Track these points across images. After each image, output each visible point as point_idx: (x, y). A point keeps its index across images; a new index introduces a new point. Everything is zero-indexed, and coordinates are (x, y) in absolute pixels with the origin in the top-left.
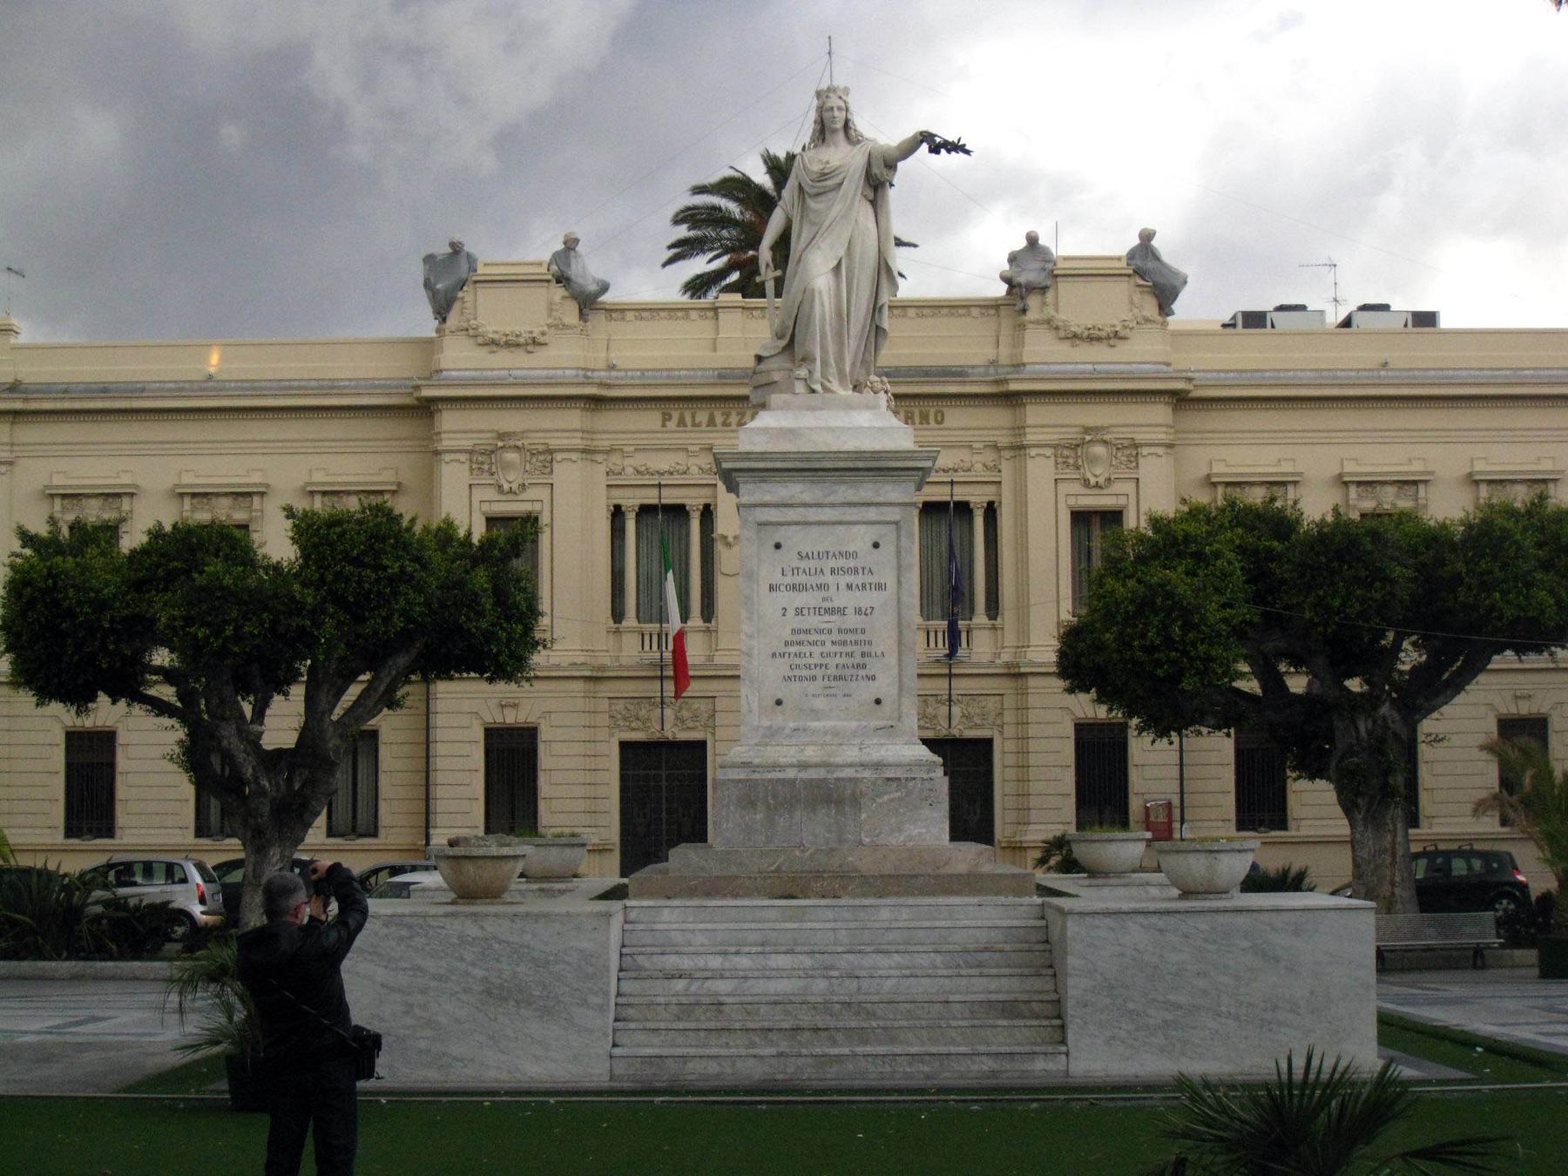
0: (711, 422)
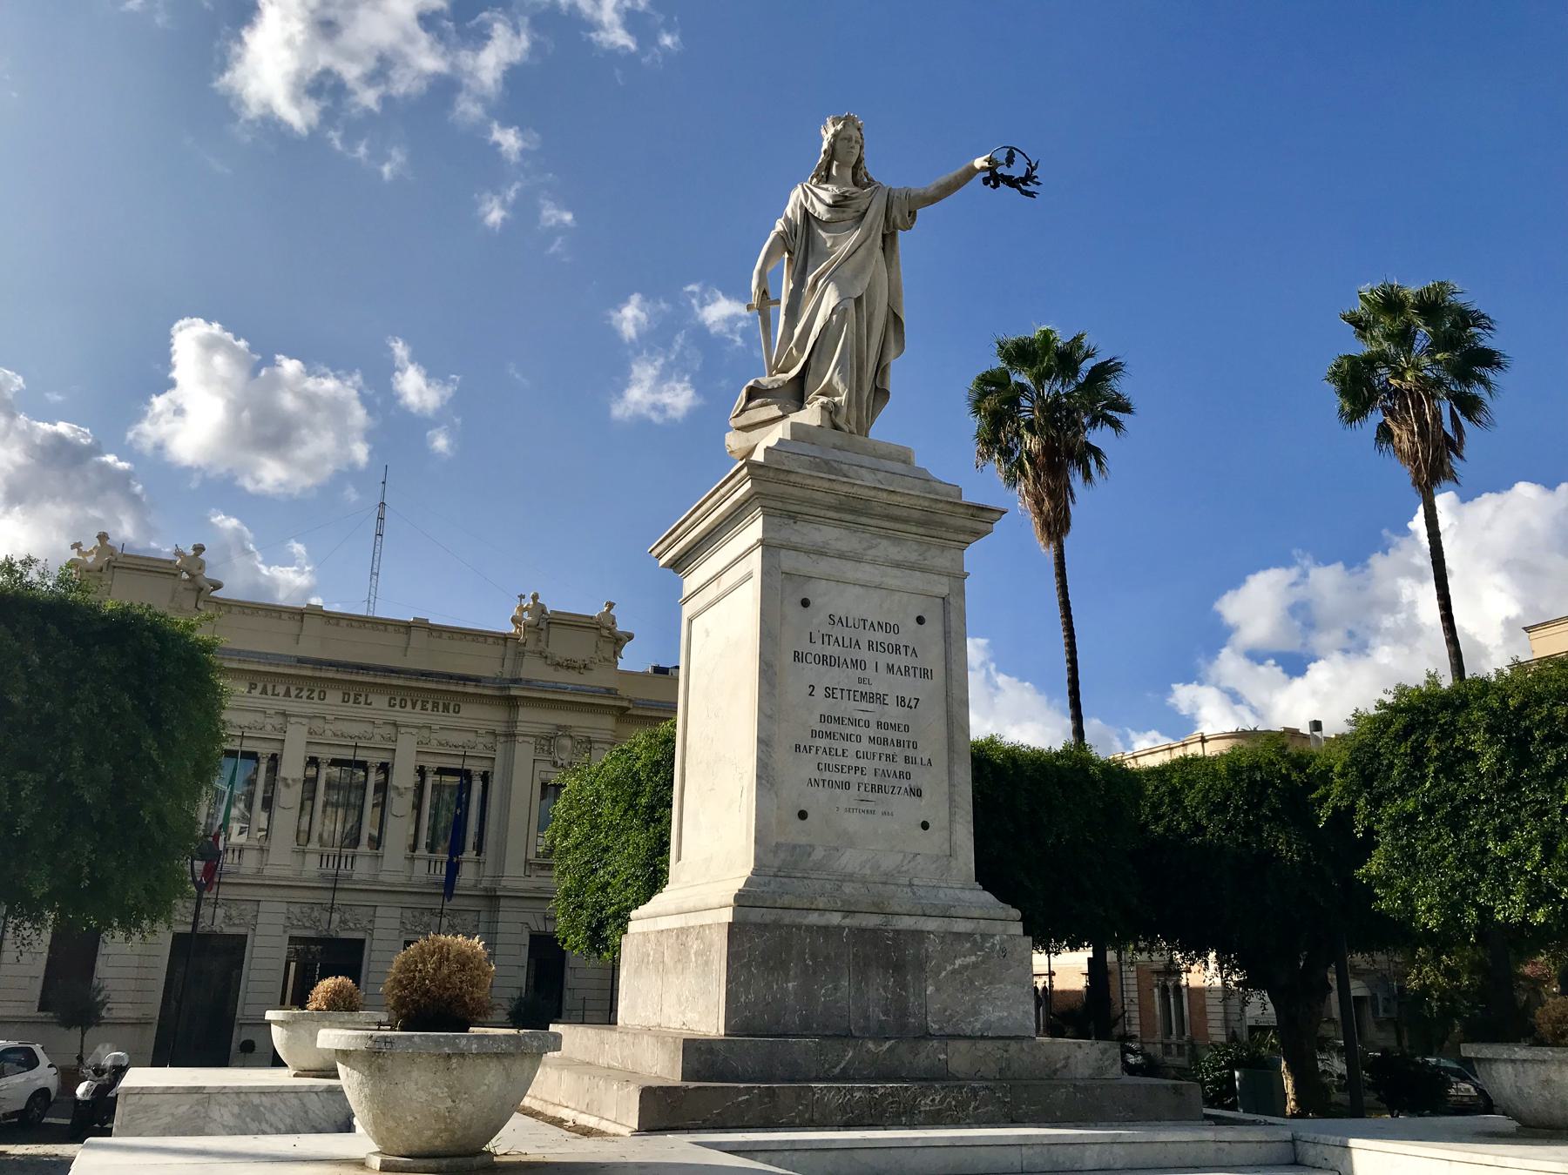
0: (287, 694)
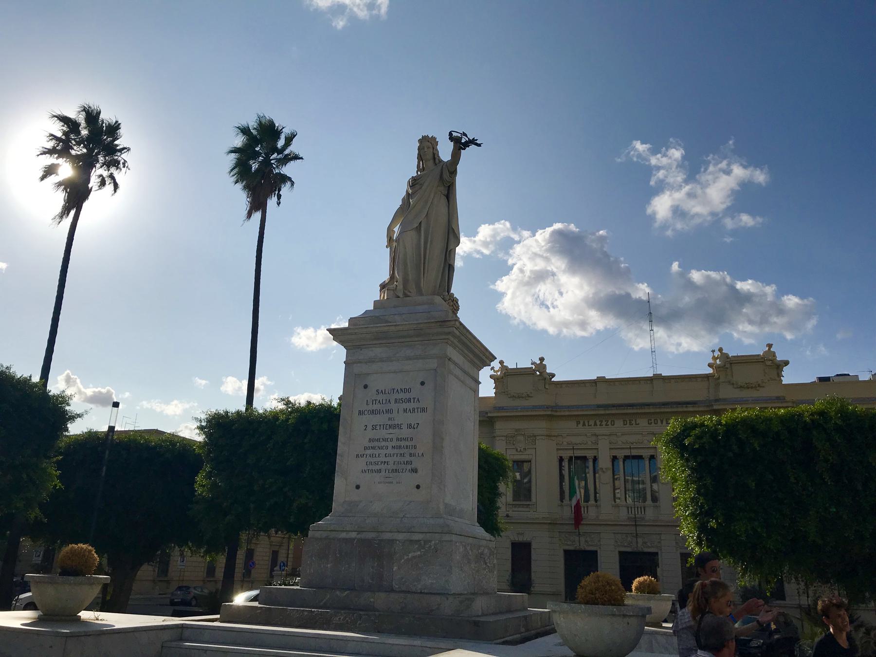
0: (595, 424)
